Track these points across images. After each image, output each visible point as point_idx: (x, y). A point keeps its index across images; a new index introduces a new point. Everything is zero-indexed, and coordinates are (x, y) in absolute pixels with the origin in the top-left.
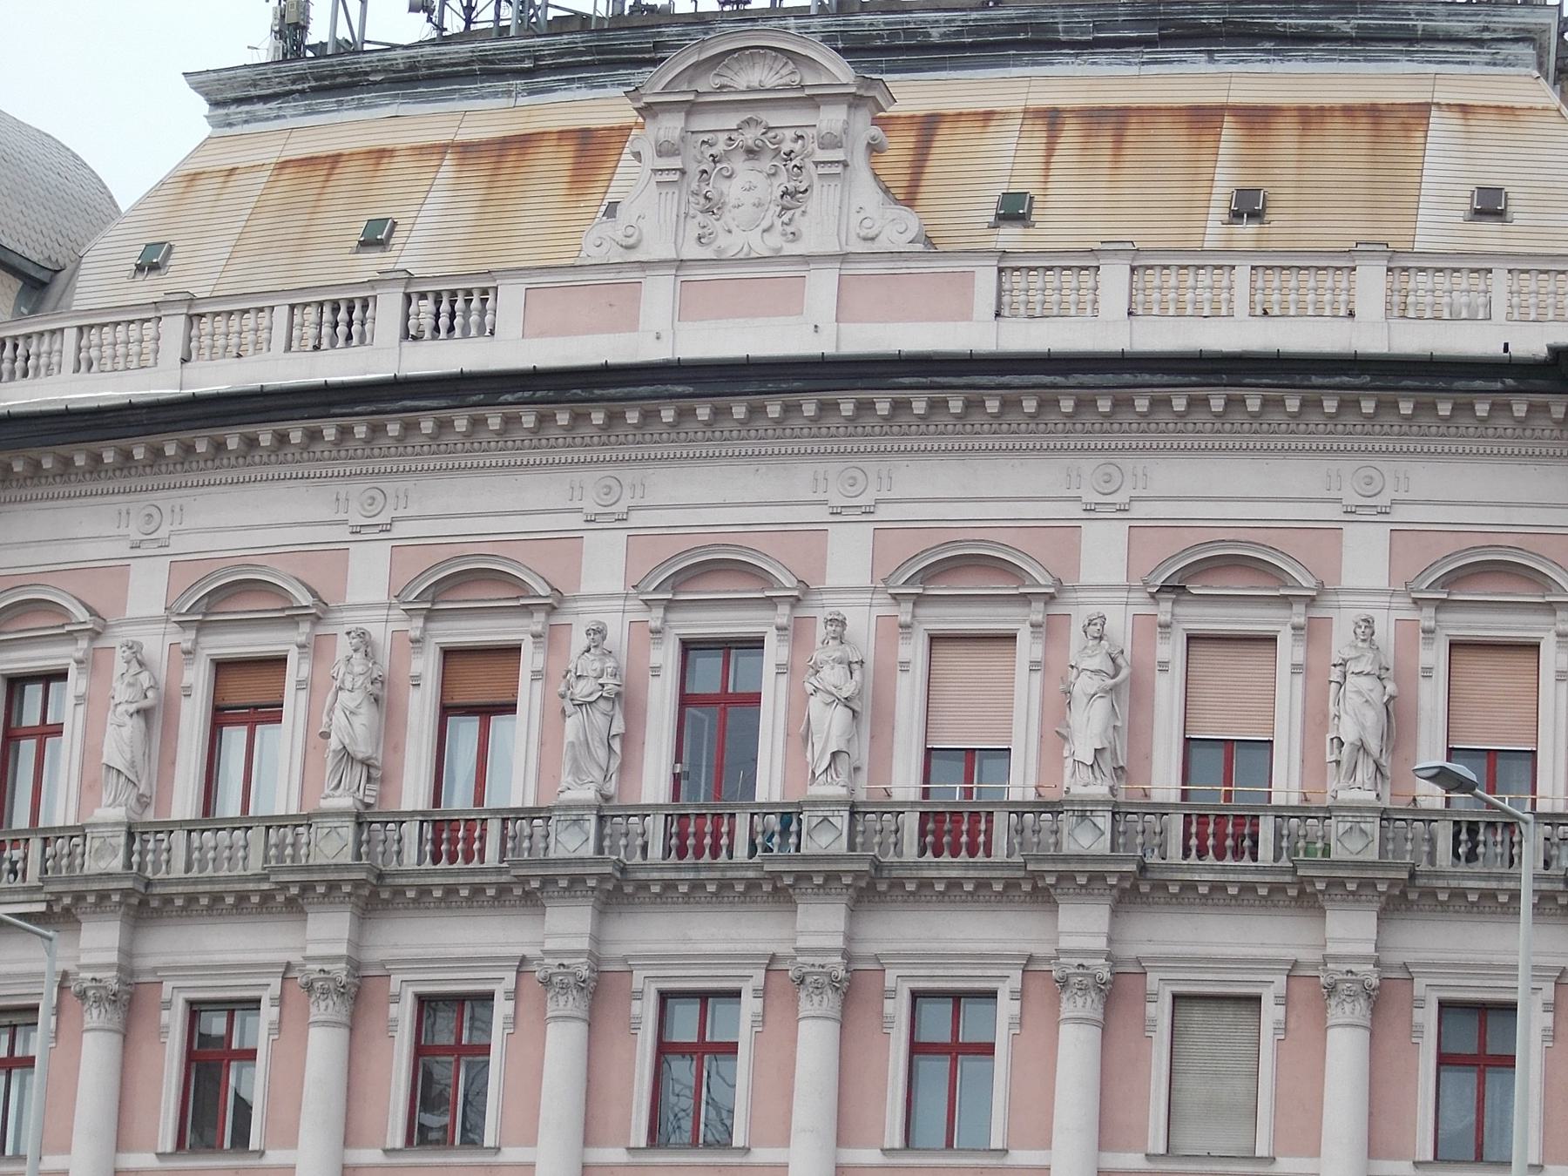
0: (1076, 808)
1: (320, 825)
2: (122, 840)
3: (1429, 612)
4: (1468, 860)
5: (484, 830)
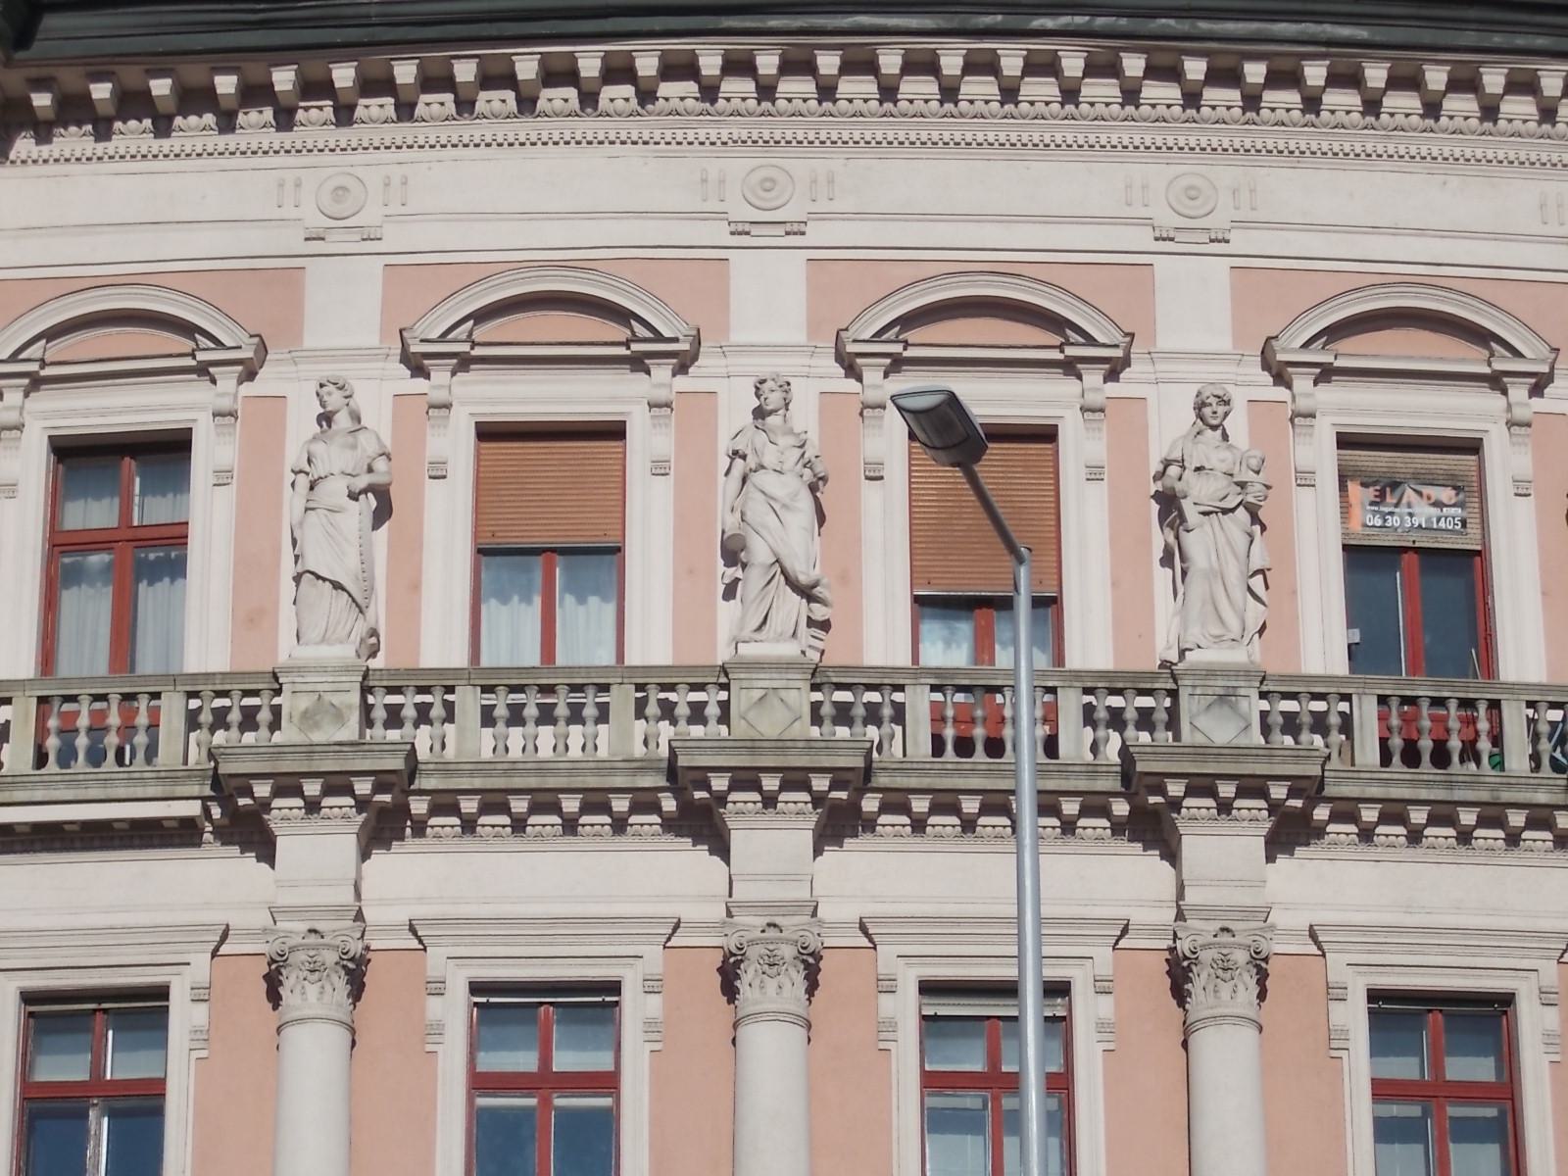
1: (745, 684)
2: (355, 698)
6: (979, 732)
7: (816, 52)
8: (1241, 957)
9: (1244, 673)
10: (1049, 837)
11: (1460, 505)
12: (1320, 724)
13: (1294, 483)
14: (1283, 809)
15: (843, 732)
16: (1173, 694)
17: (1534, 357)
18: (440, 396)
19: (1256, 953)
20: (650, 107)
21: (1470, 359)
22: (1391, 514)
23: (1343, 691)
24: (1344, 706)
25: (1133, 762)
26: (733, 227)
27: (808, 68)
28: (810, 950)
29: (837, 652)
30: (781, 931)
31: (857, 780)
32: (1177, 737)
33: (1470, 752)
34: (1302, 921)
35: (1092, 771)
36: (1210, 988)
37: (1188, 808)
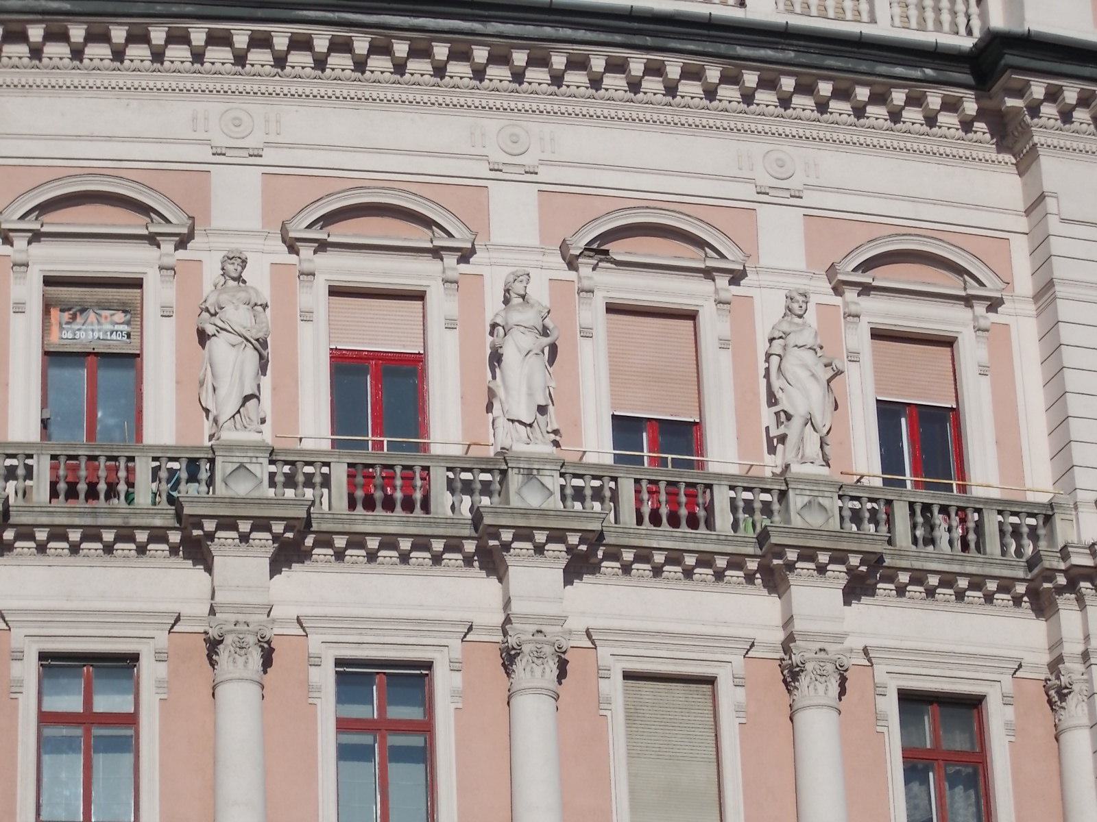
0: (522, 466)
3: (851, 294)
4: (67, 497)
5: (130, 471)
6: (378, 495)
7: (473, 47)
8: (548, 650)
9: (257, 447)
10: (93, 556)
11: (128, 323)
12: (598, 494)
13: (299, 318)
14: (575, 551)
15: (290, 493)
16: (504, 473)
17: (733, 259)
18: (20, 258)
19: (559, 648)
20: (1067, 126)
21: (134, 223)
22: (79, 330)
23: (27, 452)
24: (325, 470)
25: (481, 518)
26: (214, 150)
27: (145, 39)
28: (266, 639)
29: (568, 453)
30: (248, 626)
31: (302, 524)
32: (507, 501)
33: (112, 492)
34: (293, 612)
35: (453, 523)
36: (528, 669)
37: (219, 538)
